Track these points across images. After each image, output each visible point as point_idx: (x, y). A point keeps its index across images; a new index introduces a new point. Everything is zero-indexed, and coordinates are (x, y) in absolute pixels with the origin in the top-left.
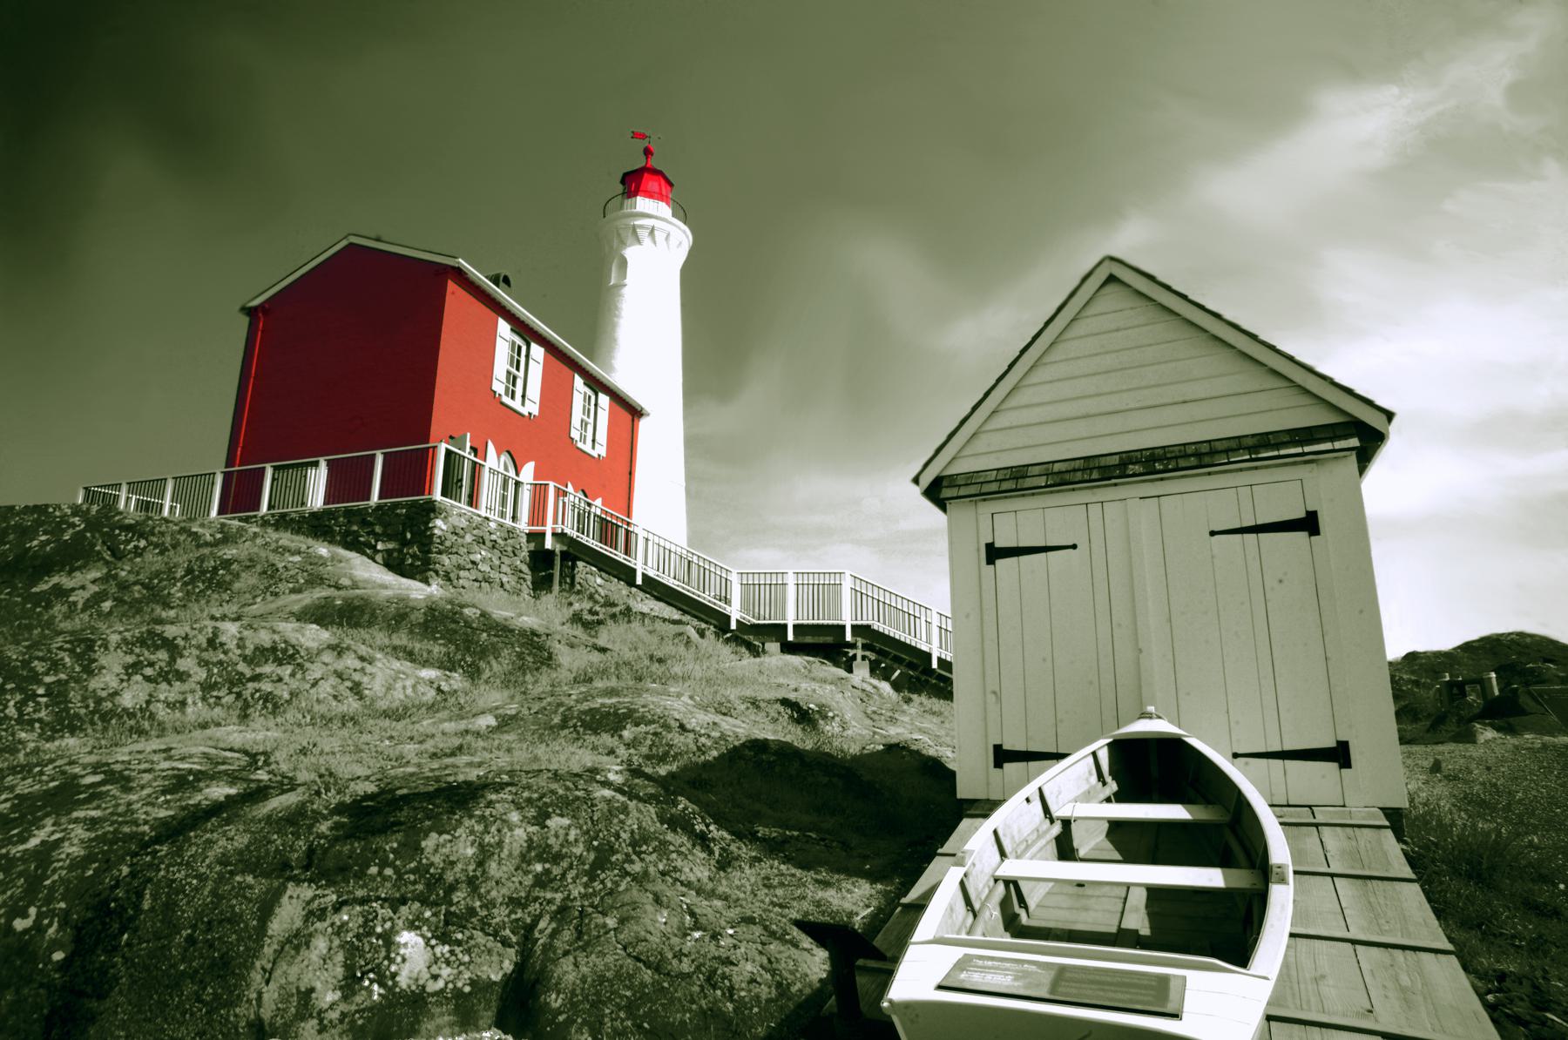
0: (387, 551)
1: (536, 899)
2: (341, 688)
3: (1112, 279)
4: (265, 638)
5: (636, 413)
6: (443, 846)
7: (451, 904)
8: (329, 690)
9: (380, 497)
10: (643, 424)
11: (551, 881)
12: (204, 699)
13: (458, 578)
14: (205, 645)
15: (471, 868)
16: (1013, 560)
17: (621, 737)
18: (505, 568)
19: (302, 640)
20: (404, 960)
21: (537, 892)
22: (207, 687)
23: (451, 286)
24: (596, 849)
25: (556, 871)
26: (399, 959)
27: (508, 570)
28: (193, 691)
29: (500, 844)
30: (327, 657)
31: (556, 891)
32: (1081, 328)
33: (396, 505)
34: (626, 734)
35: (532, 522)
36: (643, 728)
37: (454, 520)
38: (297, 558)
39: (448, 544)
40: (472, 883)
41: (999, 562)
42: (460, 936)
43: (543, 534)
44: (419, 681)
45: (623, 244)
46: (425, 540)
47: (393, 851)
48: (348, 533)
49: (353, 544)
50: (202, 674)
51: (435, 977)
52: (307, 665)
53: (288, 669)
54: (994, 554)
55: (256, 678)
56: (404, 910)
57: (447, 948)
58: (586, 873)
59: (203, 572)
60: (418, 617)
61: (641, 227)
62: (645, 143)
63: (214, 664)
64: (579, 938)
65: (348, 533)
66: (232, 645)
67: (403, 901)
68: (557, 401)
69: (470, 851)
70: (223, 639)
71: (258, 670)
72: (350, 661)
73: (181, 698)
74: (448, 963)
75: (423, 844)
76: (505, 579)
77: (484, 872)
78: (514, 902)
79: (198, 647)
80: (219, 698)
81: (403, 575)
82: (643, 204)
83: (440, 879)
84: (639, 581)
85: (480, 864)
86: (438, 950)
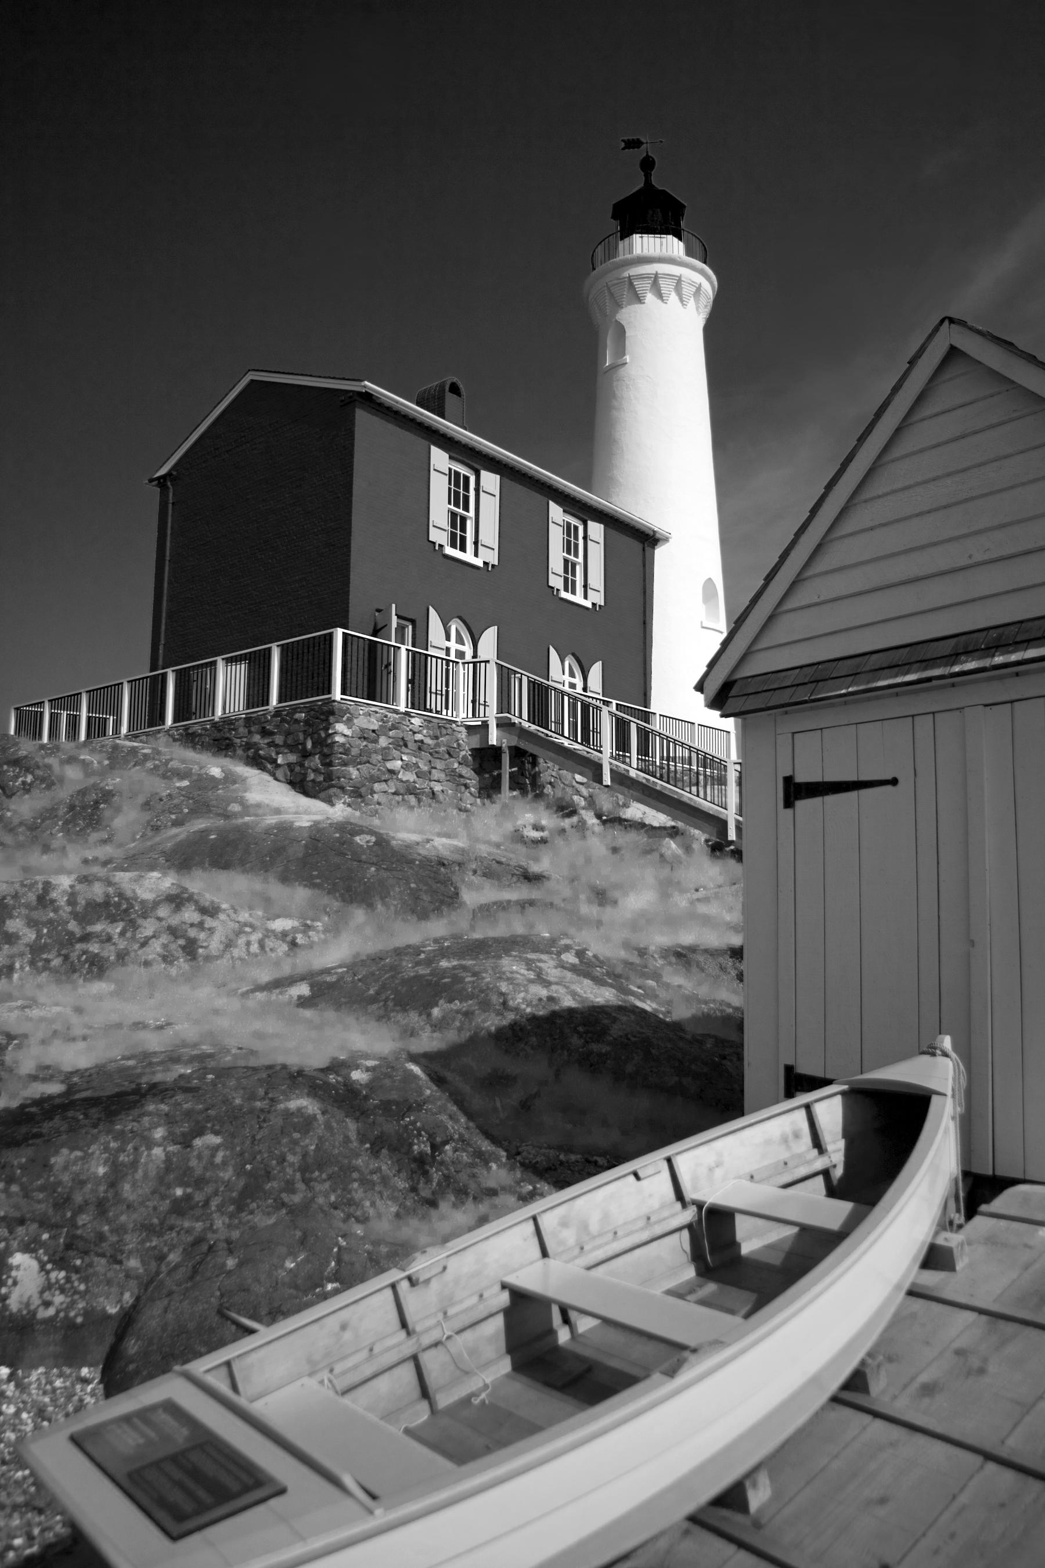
0: (289, 765)
1: (171, 1228)
2: (173, 947)
3: (953, 353)
4: (98, 891)
5: (647, 540)
6: (75, 1163)
7: (75, 1226)
8: (159, 949)
9: (280, 701)
10: (660, 553)
11: (192, 1208)
12: (32, 963)
13: (373, 792)
14: (34, 903)
15: (102, 1188)
16: (817, 801)
17: (429, 1015)
18: (436, 775)
19: (139, 892)
20: (15, 1283)
21: (173, 1220)
22: (36, 949)
23: (362, 417)
24: (250, 1174)
25: (199, 1197)
26: (10, 1282)
27: (442, 776)
28: (22, 955)
29: (134, 1164)
30: (163, 912)
31: (197, 1220)
32: (909, 443)
33: (295, 709)
34: (436, 1012)
35: (500, 710)
36: (457, 1005)
37: (361, 722)
38: (186, 783)
39: (355, 751)
40: (101, 1207)
41: (800, 804)
42: (78, 1262)
43: (485, 725)
44: (269, 933)
45: (619, 306)
46: (325, 746)
47: (22, 1167)
48: (248, 746)
49: (256, 761)
50: (30, 936)
51: (47, 1304)
52: (140, 921)
53: (118, 928)
54: (795, 791)
55: (86, 938)
56: (20, 1231)
57: (63, 1274)
58: (233, 1201)
59: (84, 808)
60: (297, 851)
61: (641, 277)
62: (640, 154)
63: (44, 924)
64: (191, 1278)
65: (248, 746)
66: (62, 901)
67: (22, 1222)
68: (523, 539)
69: (101, 1171)
70: (54, 895)
71: (90, 929)
72: (189, 915)
73: (7, 962)
74: (62, 1290)
75: (53, 1160)
76: (437, 788)
77: (117, 1194)
78: (148, 1229)
79: (27, 906)
80: (48, 961)
81: (306, 793)
82: (643, 244)
83: (68, 1199)
84: (607, 780)
85: (112, 1185)
86: (53, 1275)
